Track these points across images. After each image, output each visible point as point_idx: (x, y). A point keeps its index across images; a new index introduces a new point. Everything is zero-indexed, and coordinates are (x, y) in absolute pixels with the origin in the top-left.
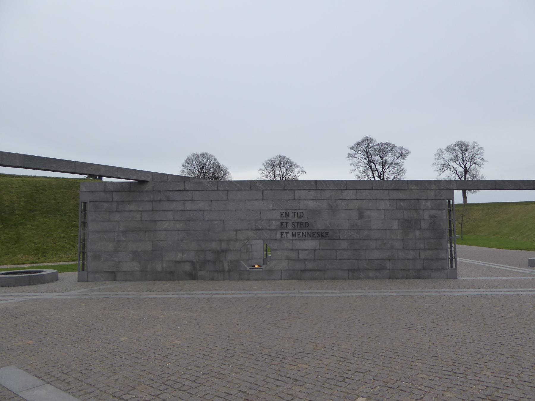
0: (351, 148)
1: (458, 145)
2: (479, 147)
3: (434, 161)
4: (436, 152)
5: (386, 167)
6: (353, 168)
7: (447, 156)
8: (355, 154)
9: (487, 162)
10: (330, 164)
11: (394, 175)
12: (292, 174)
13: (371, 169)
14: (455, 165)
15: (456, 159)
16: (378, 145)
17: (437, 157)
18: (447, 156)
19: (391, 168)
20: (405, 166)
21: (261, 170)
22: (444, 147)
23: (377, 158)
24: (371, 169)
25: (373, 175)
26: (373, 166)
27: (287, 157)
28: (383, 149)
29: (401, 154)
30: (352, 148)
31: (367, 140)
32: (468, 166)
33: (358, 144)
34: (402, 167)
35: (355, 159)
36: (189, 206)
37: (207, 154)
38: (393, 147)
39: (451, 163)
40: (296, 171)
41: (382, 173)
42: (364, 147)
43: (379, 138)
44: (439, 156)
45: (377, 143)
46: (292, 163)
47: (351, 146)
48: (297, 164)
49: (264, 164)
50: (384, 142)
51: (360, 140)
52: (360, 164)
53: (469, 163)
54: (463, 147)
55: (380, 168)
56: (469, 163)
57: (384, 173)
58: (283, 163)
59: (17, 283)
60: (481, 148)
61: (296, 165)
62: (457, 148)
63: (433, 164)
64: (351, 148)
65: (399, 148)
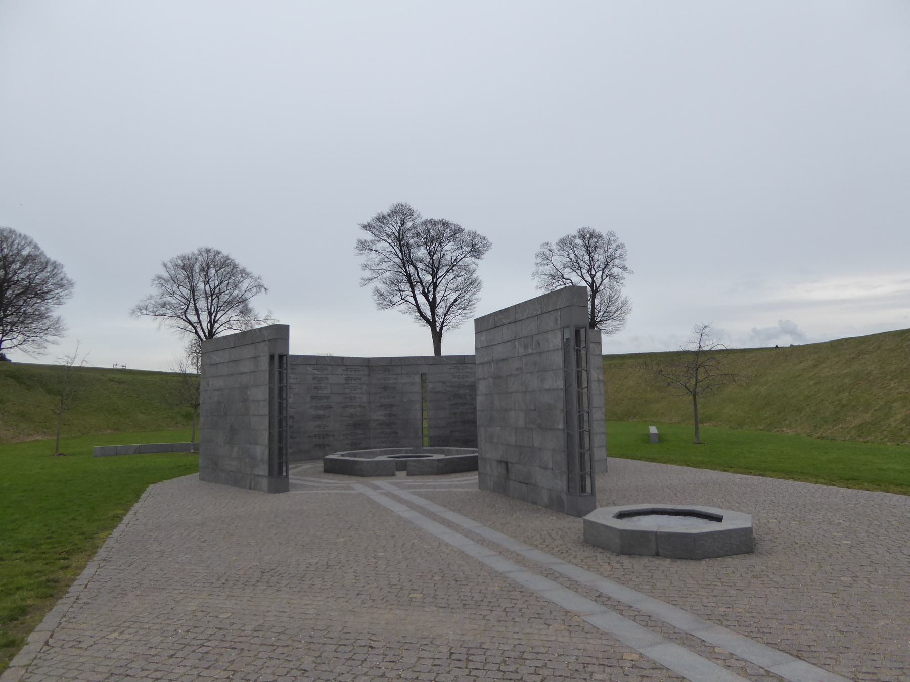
0: (365, 227)
1: (583, 237)
2: (618, 243)
4: (538, 250)
5: (442, 272)
6: (368, 274)
7: (559, 260)
8: (373, 242)
9: (633, 273)
11: (458, 293)
12: (236, 292)
13: (408, 276)
15: (575, 265)
16: (425, 223)
17: (540, 260)
18: (559, 260)
19: (451, 275)
21: (159, 278)
22: (554, 241)
23: (421, 252)
24: (408, 276)
25: (413, 291)
26: (412, 270)
27: (225, 252)
28: (437, 234)
29: (473, 245)
30: (367, 227)
31: (402, 212)
32: (598, 281)
33: (381, 219)
35: (373, 255)
36: (604, 642)
37: (12, 232)
38: (458, 231)
40: (245, 285)
41: (431, 288)
42: (393, 228)
43: (427, 210)
44: (544, 257)
45: (423, 219)
46: (235, 266)
47: (365, 223)
48: (248, 270)
49: (165, 265)
50: (436, 218)
51: (386, 211)
52: (385, 266)
53: (599, 274)
54: (590, 241)
55: (428, 278)
56: (599, 274)
57: (435, 286)
60: (621, 246)
61: (245, 274)
62: (578, 241)
63: (533, 274)
64: (365, 227)
65: (470, 234)
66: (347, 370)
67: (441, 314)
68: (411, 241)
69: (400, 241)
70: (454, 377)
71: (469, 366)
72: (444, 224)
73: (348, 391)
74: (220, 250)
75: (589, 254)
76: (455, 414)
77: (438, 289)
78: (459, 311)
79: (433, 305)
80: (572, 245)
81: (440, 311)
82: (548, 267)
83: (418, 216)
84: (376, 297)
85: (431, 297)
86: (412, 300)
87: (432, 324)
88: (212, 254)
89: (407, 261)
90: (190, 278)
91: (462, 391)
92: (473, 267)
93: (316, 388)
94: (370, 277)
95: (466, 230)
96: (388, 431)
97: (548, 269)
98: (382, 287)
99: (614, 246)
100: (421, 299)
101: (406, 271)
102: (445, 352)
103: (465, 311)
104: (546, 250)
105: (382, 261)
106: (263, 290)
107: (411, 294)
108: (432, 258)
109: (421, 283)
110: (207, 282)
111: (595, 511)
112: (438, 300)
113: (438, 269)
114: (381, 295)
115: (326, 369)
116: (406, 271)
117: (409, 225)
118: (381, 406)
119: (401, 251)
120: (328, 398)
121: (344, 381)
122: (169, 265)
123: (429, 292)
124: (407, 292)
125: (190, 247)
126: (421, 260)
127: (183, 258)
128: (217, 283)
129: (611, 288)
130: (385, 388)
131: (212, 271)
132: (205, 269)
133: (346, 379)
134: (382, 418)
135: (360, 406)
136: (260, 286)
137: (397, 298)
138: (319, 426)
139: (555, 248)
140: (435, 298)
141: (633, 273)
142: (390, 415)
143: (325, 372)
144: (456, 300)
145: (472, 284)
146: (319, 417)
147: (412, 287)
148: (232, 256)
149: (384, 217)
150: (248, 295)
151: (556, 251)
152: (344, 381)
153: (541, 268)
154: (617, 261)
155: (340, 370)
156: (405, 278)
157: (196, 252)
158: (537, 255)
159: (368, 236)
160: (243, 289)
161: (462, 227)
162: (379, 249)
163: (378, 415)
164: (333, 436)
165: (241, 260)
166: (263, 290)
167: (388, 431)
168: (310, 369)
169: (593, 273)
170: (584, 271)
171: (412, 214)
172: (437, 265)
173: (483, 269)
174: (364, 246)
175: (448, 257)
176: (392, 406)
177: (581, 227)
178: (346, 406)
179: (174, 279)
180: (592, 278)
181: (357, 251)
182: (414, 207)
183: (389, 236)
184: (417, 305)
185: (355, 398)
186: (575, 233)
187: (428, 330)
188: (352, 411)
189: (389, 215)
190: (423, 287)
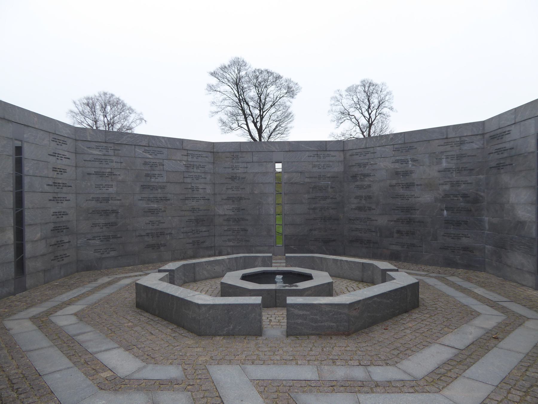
5: (267, 107)
6: (215, 109)
7: (347, 102)
9: (397, 111)
10: (185, 112)
11: (278, 122)
13: (243, 110)
14: (358, 114)
17: (333, 102)
19: (273, 110)
21: (72, 112)
22: (343, 88)
24: (243, 110)
25: (246, 121)
27: (117, 95)
28: (263, 80)
29: (289, 88)
30: (213, 74)
32: (373, 117)
33: (224, 68)
34: (289, 111)
38: (278, 77)
39: (352, 110)
41: (259, 120)
42: (232, 75)
43: (256, 62)
44: (337, 100)
45: (254, 69)
46: (124, 105)
47: (212, 71)
48: (133, 108)
49: (75, 103)
51: (227, 63)
52: (226, 103)
54: (369, 89)
55: (256, 112)
57: (262, 117)
58: (111, 103)
59: (499, 149)
62: (360, 89)
66: (187, 155)
67: (266, 137)
68: (245, 86)
69: (237, 84)
70: (314, 166)
71: (332, 153)
72: (268, 72)
73: (189, 180)
74: (113, 93)
76: (314, 209)
77: (264, 119)
78: (279, 135)
84: (220, 124)
85: (258, 125)
88: (108, 96)
89: (242, 101)
90: (94, 112)
91: (323, 183)
92: (288, 104)
93: (147, 175)
94: (216, 110)
95: (284, 78)
96: (236, 228)
97: (339, 108)
98: (225, 118)
99: (385, 93)
100: (252, 126)
101: (241, 107)
103: (282, 136)
106: (143, 121)
107: (245, 123)
109: (252, 116)
110: (105, 116)
112: (264, 127)
113: (264, 105)
114: (224, 123)
115: (161, 153)
116: (241, 107)
117: (243, 73)
118: (228, 199)
119: (238, 92)
120: (163, 188)
121: (183, 169)
122: (78, 103)
123: (257, 122)
124: (242, 122)
125: (93, 91)
126: (252, 99)
127: (88, 98)
128: (112, 116)
130: (233, 178)
131: (108, 108)
132: (104, 108)
133: (187, 166)
134: (231, 213)
135: (204, 198)
136: (141, 119)
137: (235, 126)
138: (152, 223)
139: (344, 93)
140: (261, 126)
141: (397, 111)
142: (238, 209)
143: (159, 156)
144: (276, 127)
145: (287, 116)
146: (152, 211)
147: (246, 119)
148: (122, 98)
149: (225, 67)
150: (133, 125)
151: (344, 96)
152: (183, 169)
153: (334, 108)
154: (386, 104)
155: (178, 155)
156: (240, 112)
157: (97, 95)
158: (332, 98)
159: (214, 81)
160: (130, 121)
161: (281, 75)
162: (221, 90)
163: (225, 210)
164: (171, 234)
165: (129, 102)
166: (143, 121)
167: (236, 228)
168: (139, 151)
169: (370, 111)
170: (364, 110)
171: (245, 65)
172: (263, 101)
173: (295, 105)
174: (211, 88)
175: (271, 96)
176: (240, 199)
178: (186, 199)
179: (82, 113)
181: (207, 92)
185: (198, 189)
186: (359, 83)
188: (194, 204)
189: (229, 66)
190: (253, 118)
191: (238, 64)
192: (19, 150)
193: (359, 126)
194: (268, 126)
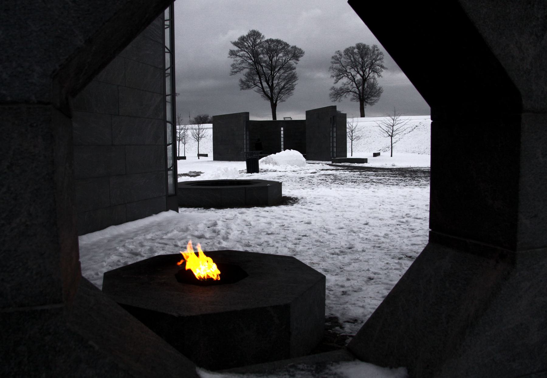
3: (331, 65)
4: (334, 54)
8: (238, 51)
17: (333, 60)
20: (298, 71)
22: (342, 50)
23: (265, 58)
29: (294, 54)
30: (235, 44)
31: (255, 34)
33: (243, 39)
35: (238, 58)
43: (268, 34)
45: (266, 39)
52: (243, 65)
62: (356, 50)
63: (330, 68)
65: (292, 47)
75: (362, 59)
79: (272, 88)
80: (353, 53)
81: (276, 91)
82: (338, 65)
83: (263, 36)
84: (240, 83)
86: (260, 85)
87: (271, 99)
89: (257, 62)
92: (295, 65)
100: (265, 84)
101: (256, 69)
102: (278, 118)
104: (338, 55)
105: (242, 62)
108: (271, 60)
109: (265, 75)
111: (428, 227)
112: (274, 85)
123: (269, 80)
126: (265, 62)
129: (374, 79)
140: (273, 84)
144: (284, 85)
147: (260, 78)
153: (335, 65)
159: (236, 48)
174: (232, 53)
177: (358, 42)
180: (363, 73)
182: (260, 31)
183: (247, 48)
184: (263, 88)
187: (268, 103)
191: (255, 34)
192: (391, 156)
193: (355, 82)
194: (278, 84)
